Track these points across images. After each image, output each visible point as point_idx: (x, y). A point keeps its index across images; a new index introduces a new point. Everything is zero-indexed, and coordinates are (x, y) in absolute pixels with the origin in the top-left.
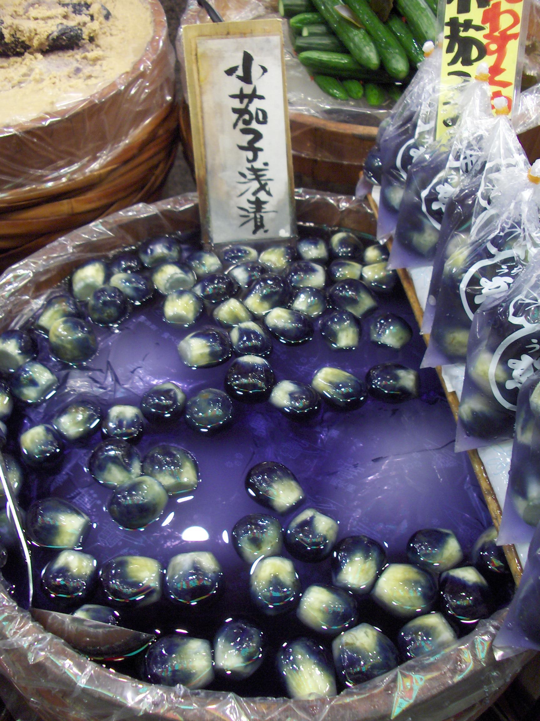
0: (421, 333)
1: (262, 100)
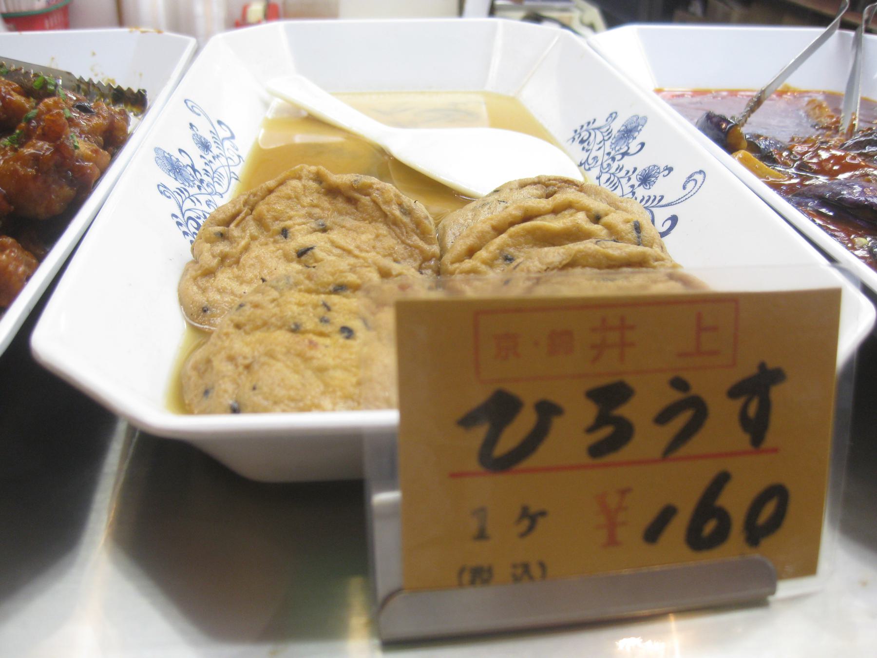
0: (135, 91)
1: (199, 117)
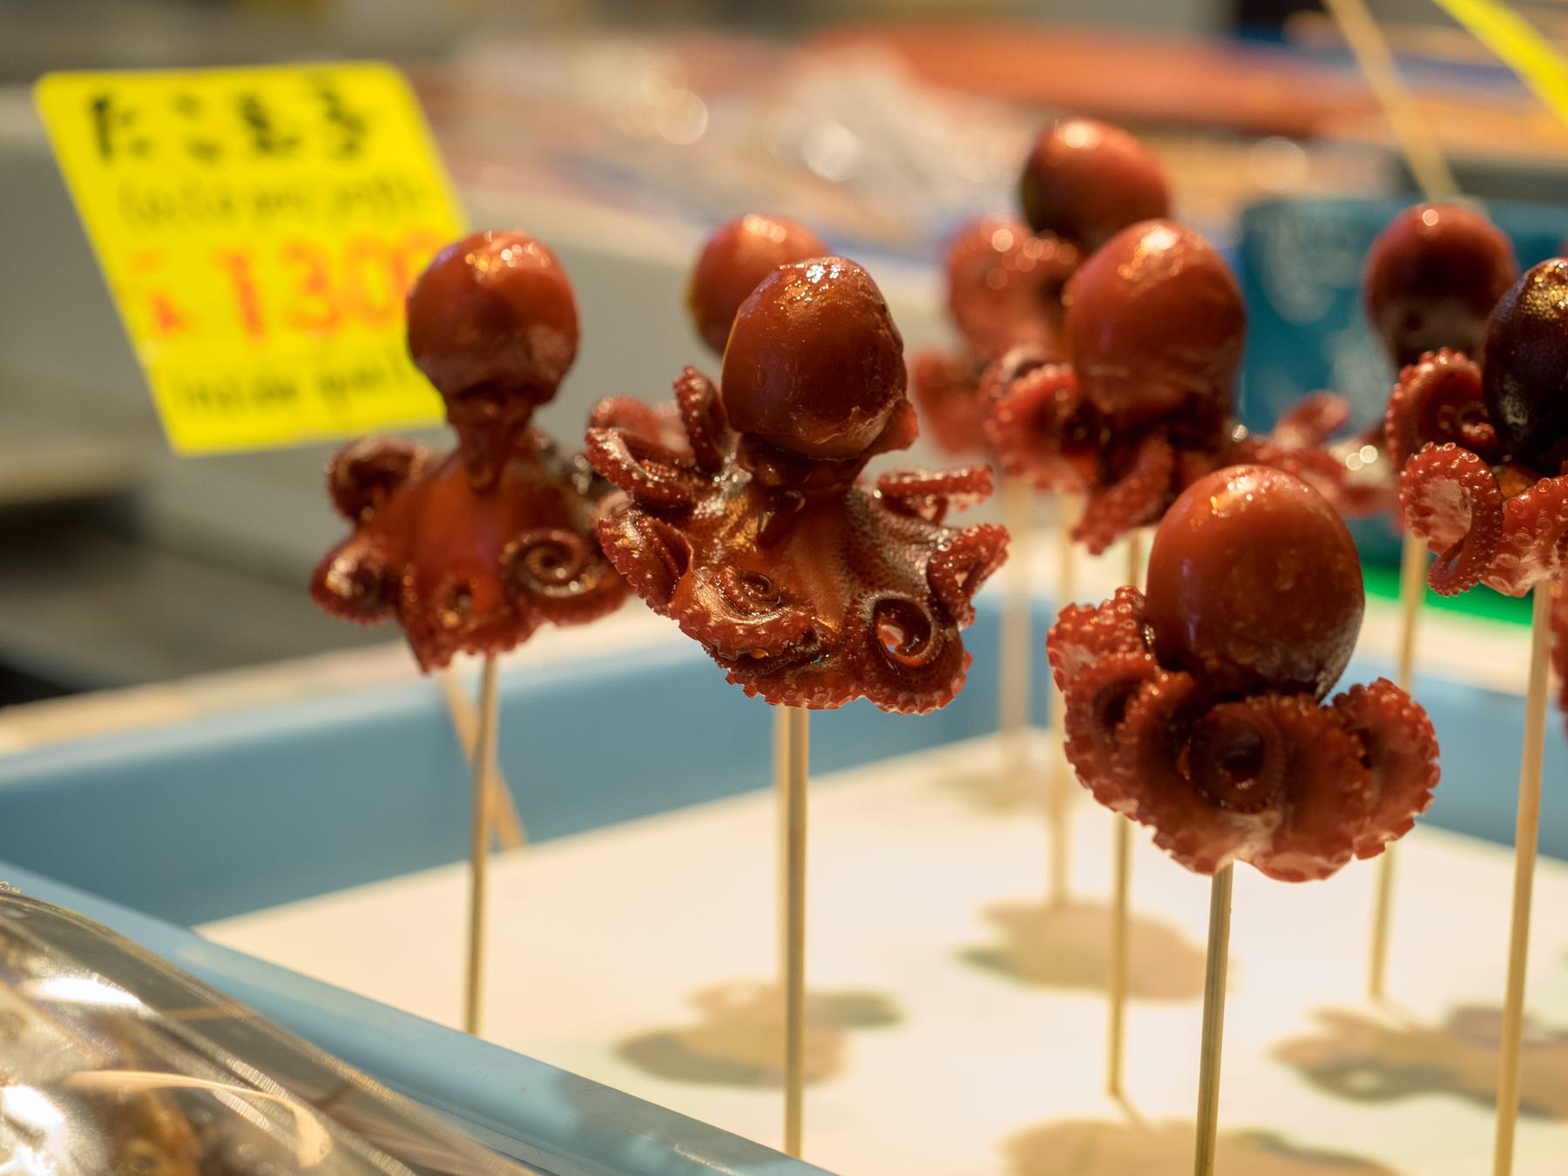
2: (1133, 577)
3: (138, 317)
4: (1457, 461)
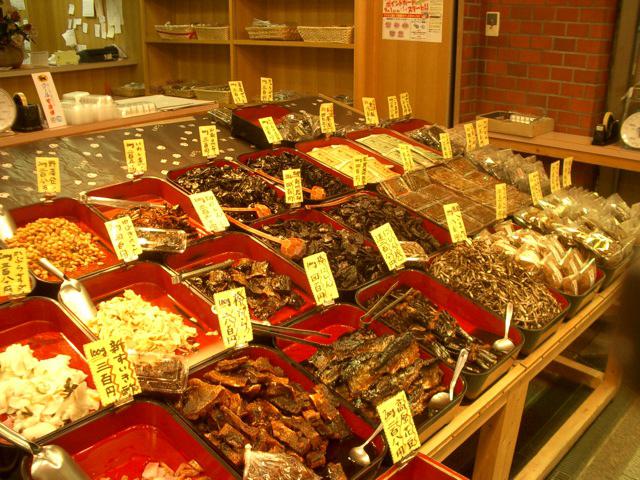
0: (140, 296)
2: (431, 452)
3: (381, 250)
4: (280, 29)
